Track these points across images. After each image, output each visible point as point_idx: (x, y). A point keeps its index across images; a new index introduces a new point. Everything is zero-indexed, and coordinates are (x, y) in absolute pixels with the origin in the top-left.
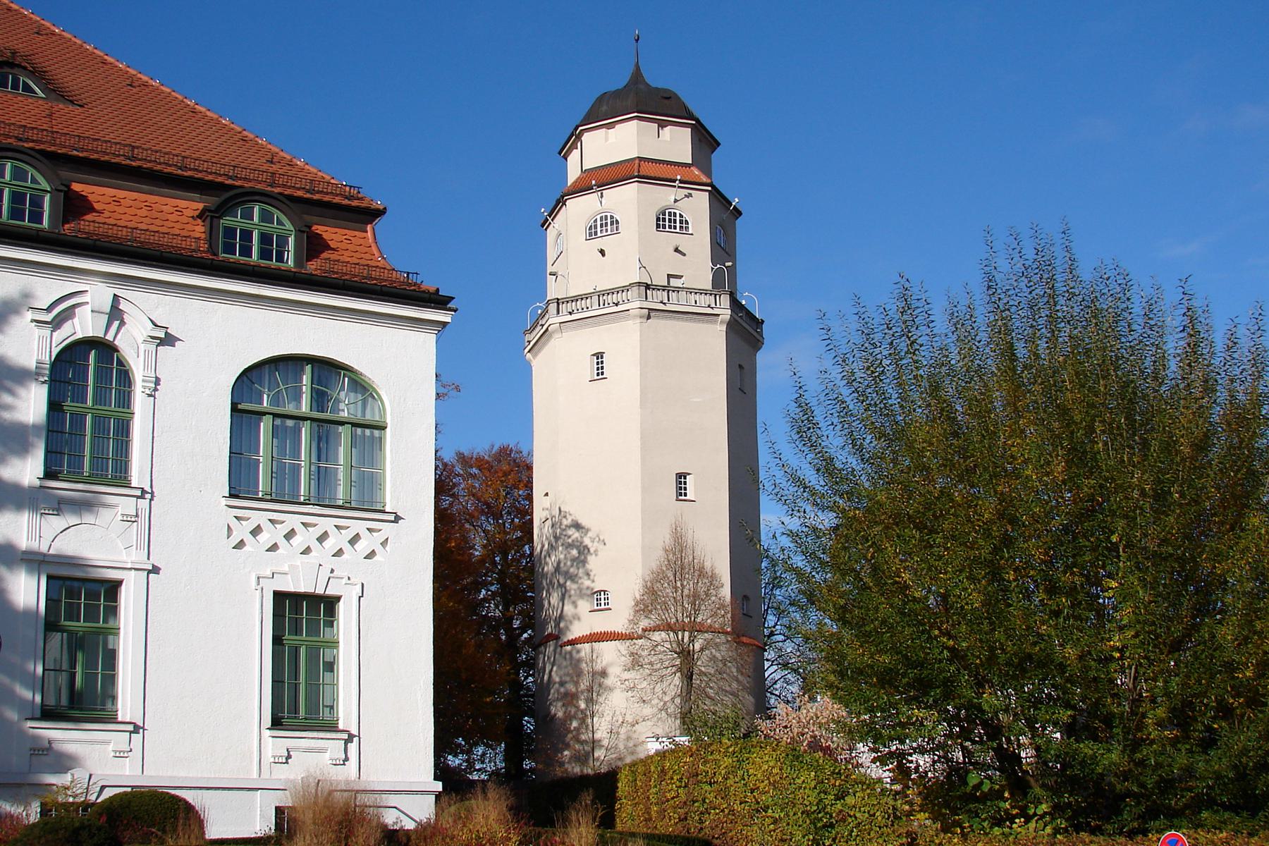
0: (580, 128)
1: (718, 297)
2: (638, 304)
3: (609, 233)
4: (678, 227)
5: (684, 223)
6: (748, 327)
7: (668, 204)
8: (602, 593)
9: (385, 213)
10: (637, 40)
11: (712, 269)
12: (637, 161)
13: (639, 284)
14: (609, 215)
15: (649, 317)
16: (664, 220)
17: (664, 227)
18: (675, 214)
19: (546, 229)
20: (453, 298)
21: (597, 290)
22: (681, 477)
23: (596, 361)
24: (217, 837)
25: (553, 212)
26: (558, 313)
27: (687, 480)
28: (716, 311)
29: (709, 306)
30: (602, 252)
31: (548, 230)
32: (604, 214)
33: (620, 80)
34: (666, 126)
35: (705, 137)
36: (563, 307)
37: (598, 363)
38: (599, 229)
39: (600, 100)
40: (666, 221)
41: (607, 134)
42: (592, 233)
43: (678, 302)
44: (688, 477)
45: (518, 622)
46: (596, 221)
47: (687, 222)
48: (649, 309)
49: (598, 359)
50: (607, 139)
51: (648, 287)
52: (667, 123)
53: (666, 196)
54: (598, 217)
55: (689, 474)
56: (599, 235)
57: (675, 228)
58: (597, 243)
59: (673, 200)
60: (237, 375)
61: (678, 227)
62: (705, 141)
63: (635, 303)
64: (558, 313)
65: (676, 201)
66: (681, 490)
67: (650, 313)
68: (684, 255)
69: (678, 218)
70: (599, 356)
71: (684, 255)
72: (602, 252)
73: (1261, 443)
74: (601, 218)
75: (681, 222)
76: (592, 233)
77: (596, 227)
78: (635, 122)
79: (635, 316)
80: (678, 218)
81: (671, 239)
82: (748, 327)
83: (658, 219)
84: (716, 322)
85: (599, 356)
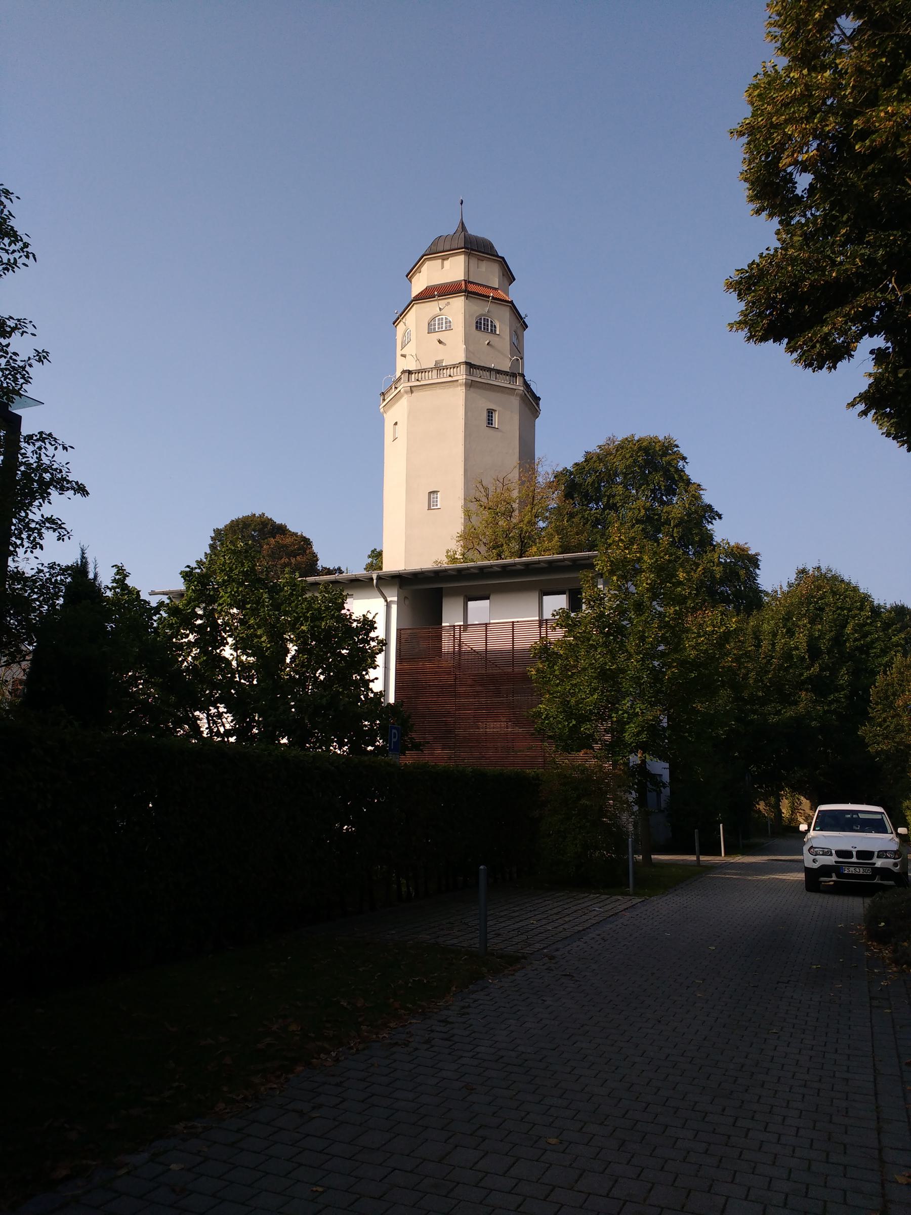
0: (425, 257)
3: (444, 329)
4: (444, 319)
6: (532, 401)
10: (462, 203)
11: (511, 359)
12: (463, 282)
15: (412, 392)
17: (481, 328)
18: (488, 320)
19: (396, 327)
20: (18, 355)
26: (409, 380)
28: (454, 379)
31: (398, 327)
33: (450, 228)
34: (483, 261)
38: (437, 327)
39: (436, 242)
41: (443, 264)
43: (427, 379)
51: (410, 372)
52: (483, 258)
56: (437, 330)
57: (484, 319)
58: (435, 336)
59: (439, 310)
60: (406, 416)
61: (444, 319)
64: (409, 380)
66: (490, 421)
67: (412, 390)
69: (489, 323)
73: (2, 457)
75: (491, 325)
80: (489, 323)
81: (485, 338)
82: (532, 401)
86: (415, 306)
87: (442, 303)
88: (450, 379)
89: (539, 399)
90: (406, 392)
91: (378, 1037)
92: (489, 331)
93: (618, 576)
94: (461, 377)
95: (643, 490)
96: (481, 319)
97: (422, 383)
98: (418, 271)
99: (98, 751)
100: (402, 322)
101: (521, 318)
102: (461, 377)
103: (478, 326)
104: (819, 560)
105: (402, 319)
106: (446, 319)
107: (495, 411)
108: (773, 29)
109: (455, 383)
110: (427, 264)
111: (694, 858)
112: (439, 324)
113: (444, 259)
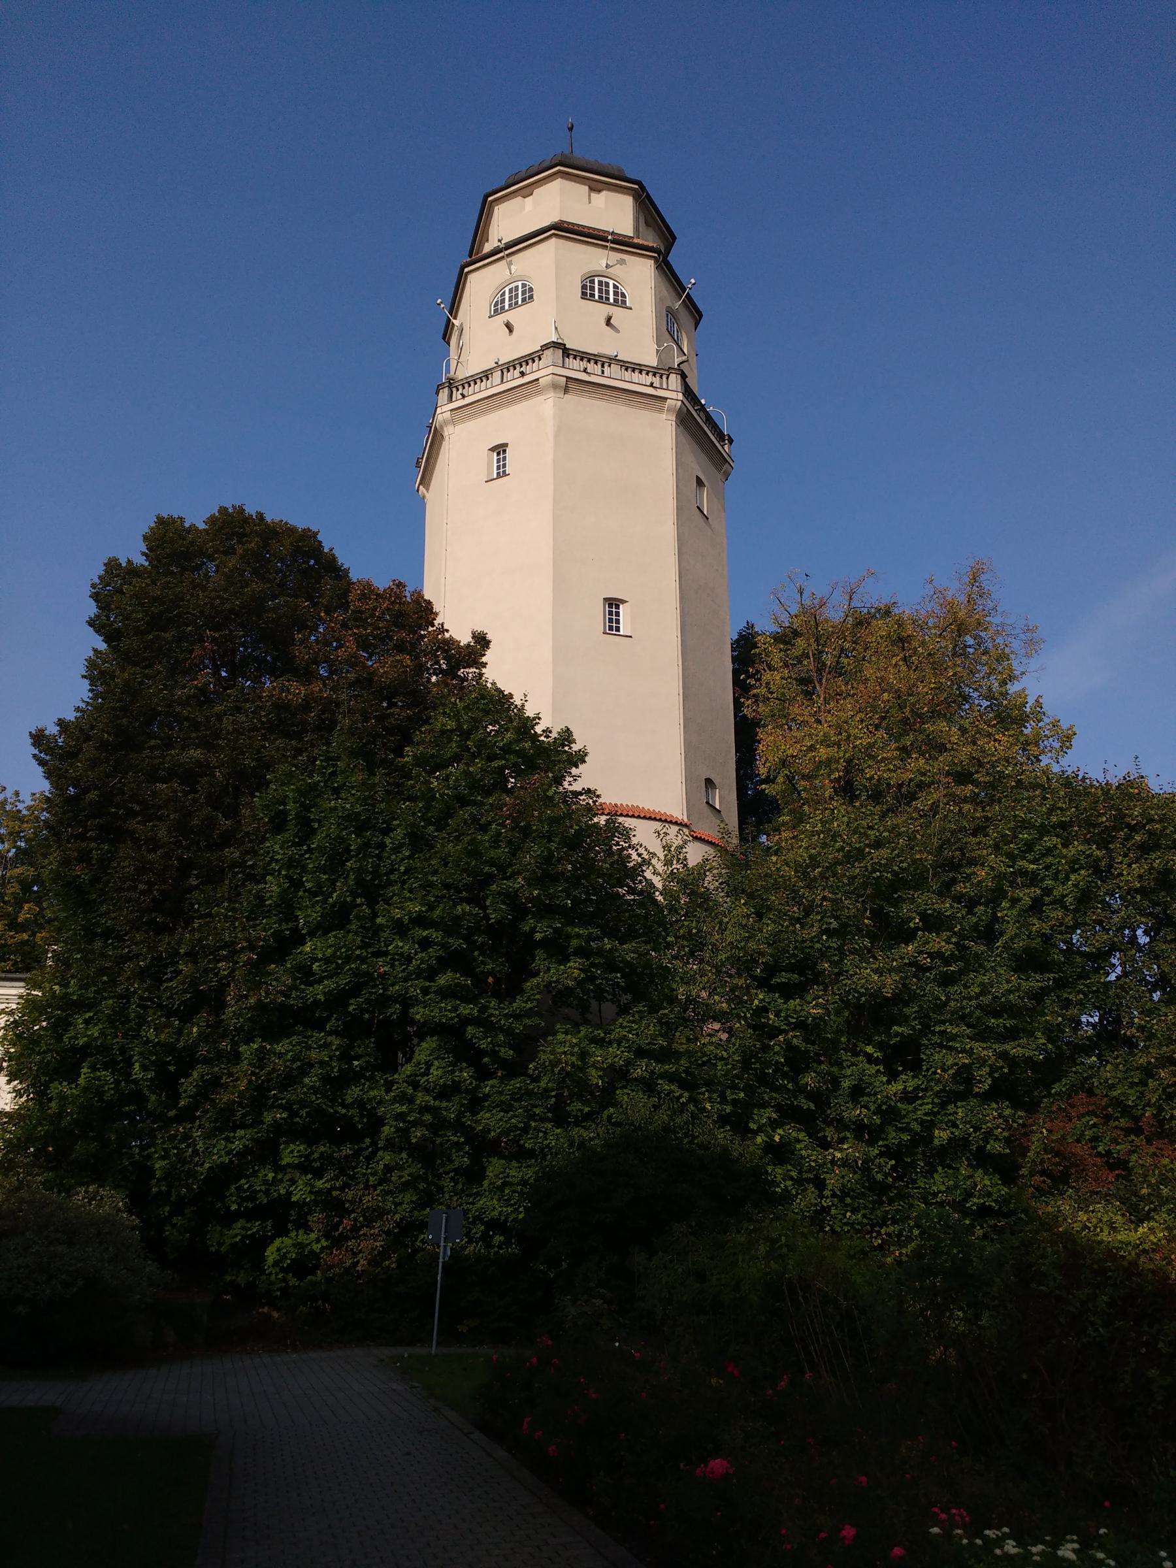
2: (551, 370)
5: (620, 301)
7: (599, 268)
10: (571, 129)
14: (520, 284)
15: (566, 390)
16: (592, 289)
17: (608, 299)
18: (607, 285)
21: (500, 363)
22: (613, 604)
23: (495, 458)
25: (454, 308)
27: (621, 610)
30: (509, 327)
32: (513, 285)
34: (599, 191)
35: (656, 222)
37: (498, 460)
42: (498, 309)
44: (621, 607)
45: (391, 1010)
46: (503, 294)
47: (623, 295)
48: (567, 377)
49: (498, 454)
51: (566, 352)
52: (600, 186)
53: (597, 259)
54: (507, 289)
57: (600, 283)
62: (646, 206)
63: (546, 370)
65: (607, 266)
66: (612, 625)
68: (618, 331)
70: (500, 449)
71: (618, 331)
72: (509, 327)
74: (511, 291)
75: (616, 293)
76: (498, 309)
77: (503, 301)
83: (584, 287)
84: (661, 410)
85: (500, 449)
86: (554, 240)
87: (615, 256)
88: (650, 391)
90: (555, 386)
93: (884, 1256)
94: (673, 395)
95: (826, 809)
96: (592, 282)
97: (467, 400)
98: (594, 184)
99: (91, 1134)
100: (503, 263)
102: (673, 395)
103: (586, 293)
104: (525, 696)
105: (508, 255)
107: (623, 602)
109: (658, 404)
110: (558, 184)
112: (607, 292)
113: (595, 188)
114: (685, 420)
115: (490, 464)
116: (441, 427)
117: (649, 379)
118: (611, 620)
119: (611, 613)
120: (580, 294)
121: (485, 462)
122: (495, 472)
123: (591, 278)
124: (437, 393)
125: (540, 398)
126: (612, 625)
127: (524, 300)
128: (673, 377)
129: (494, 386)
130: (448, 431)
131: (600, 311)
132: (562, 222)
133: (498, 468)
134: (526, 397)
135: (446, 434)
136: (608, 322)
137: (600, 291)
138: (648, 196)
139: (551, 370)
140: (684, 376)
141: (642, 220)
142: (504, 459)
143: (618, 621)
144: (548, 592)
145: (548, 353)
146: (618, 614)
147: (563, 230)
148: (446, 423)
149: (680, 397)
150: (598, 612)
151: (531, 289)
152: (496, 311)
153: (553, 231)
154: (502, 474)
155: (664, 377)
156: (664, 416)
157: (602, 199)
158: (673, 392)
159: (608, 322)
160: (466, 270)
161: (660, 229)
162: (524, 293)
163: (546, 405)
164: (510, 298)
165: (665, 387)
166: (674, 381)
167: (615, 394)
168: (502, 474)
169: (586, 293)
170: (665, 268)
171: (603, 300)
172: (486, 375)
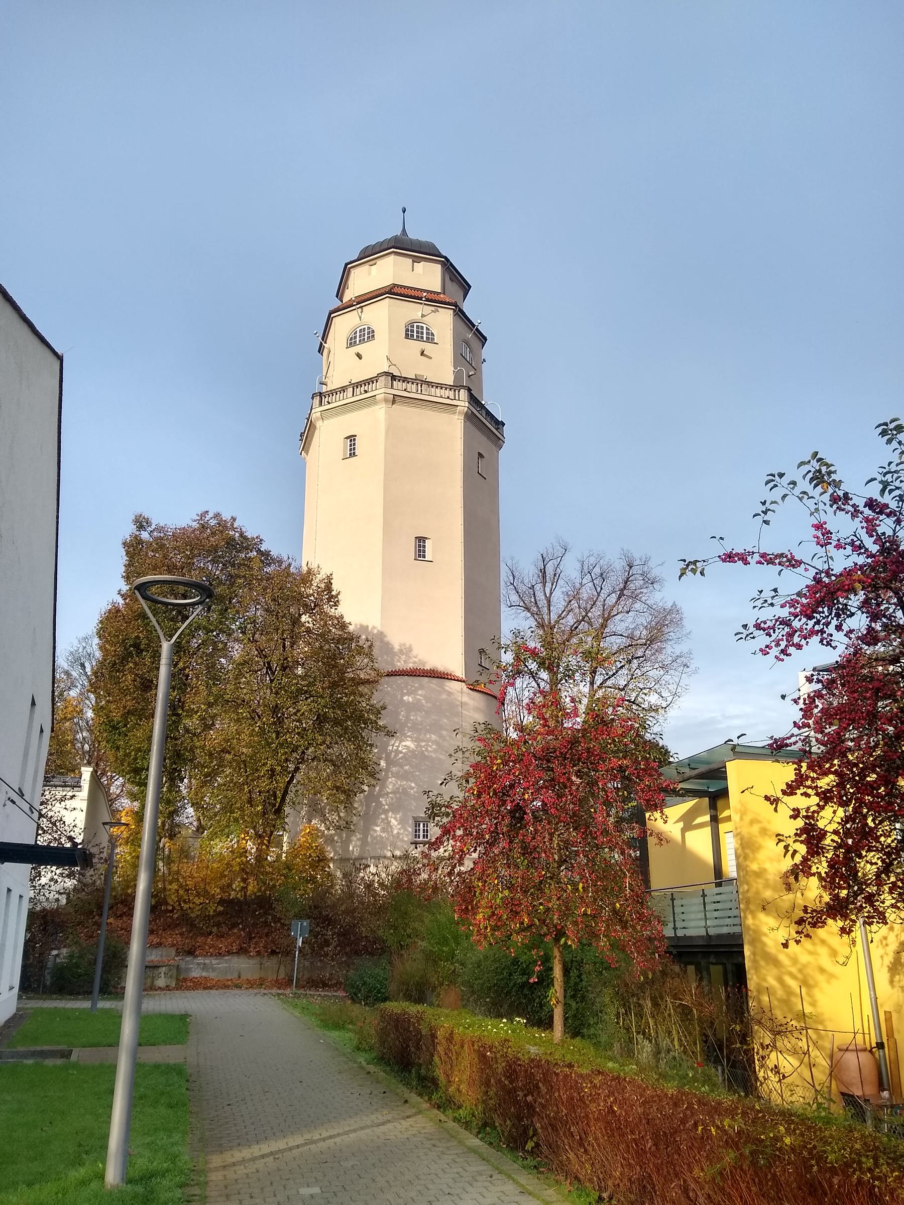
1: (457, 391)
2: (383, 390)
4: (425, 328)
5: (430, 339)
8: (425, 339)
9: (745, 564)
13: (386, 374)
14: (366, 327)
15: (394, 402)
16: (412, 331)
17: (422, 338)
18: (422, 328)
23: (349, 443)
24: (415, 409)
27: (426, 544)
28: (454, 403)
29: (448, 398)
30: (359, 356)
35: (457, 278)
36: (325, 400)
37: (351, 445)
40: (413, 332)
42: (351, 343)
47: (433, 334)
49: (351, 441)
50: (370, 273)
51: (394, 378)
53: (414, 311)
54: (358, 330)
55: (426, 538)
61: (425, 328)
62: (449, 268)
63: (380, 390)
65: (423, 316)
66: (420, 553)
67: (395, 400)
68: (431, 358)
69: (425, 331)
70: (352, 438)
71: (431, 358)
72: (359, 356)
74: (360, 331)
75: (428, 334)
76: (351, 343)
77: (355, 337)
78: (392, 257)
79: (380, 401)
80: (425, 331)
83: (407, 330)
84: (454, 413)
85: (352, 438)
87: (428, 309)
89: (499, 424)
90: (386, 400)
91: (826, 1172)
92: (425, 339)
94: (462, 404)
96: (413, 326)
98: (453, 277)
101: (474, 326)
102: (462, 404)
103: (408, 335)
106: (369, 328)
108: (480, 1136)
110: (392, 257)
111: (86, 1004)
112: (422, 333)
113: (416, 260)
114: (470, 418)
115: (345, 447)
116: (315, 421)
117: (447, 393)
118: (420, 551)
119: (420, 546)
120: (404, 336)
121: (339, 447)
122: (349, 452)
123: (411, 324)
124: (313, 398)
125: (377, 407)
126: (420, 553)
127: (368, 338)
128: (462, 391)
129: (349, 397)
130: (319, 424)
131: (417, 346)
132: (395, 285)
133: (350, 450)
134: (369, 406)
135: (317, 426)
136: (422, 354)
137: (418, 332)
138: (451, 264)
139: (383, 390)
140: (469, 390)
141: (447, 278)
142: (354, 444)
143: (424, 551)
144: (380, 545)
145: (382, 379)
146: (424, 547)
147: (394, 292)
148: (317, 419)
149: (467, 404)
150: (411, 547)
151: (373, 331)
152: (351, 344)
153: (387, 295)
154: (353, 455)
155: (457, 391)
156: (456, 417)
157: (420, 267)
158: (463, 402)
159: (422, 354)
160: (332, 315)
161: (459, 280)
162: (369, 333)
163: (380, 412)
164: (360, 336)
165: (457, 398)
166: (463, 394)
167: (425, 403)
168: (353, 455)
169: (408, 335)
170: (460, 314)
171: (419, 338)
172: (343, 389)
